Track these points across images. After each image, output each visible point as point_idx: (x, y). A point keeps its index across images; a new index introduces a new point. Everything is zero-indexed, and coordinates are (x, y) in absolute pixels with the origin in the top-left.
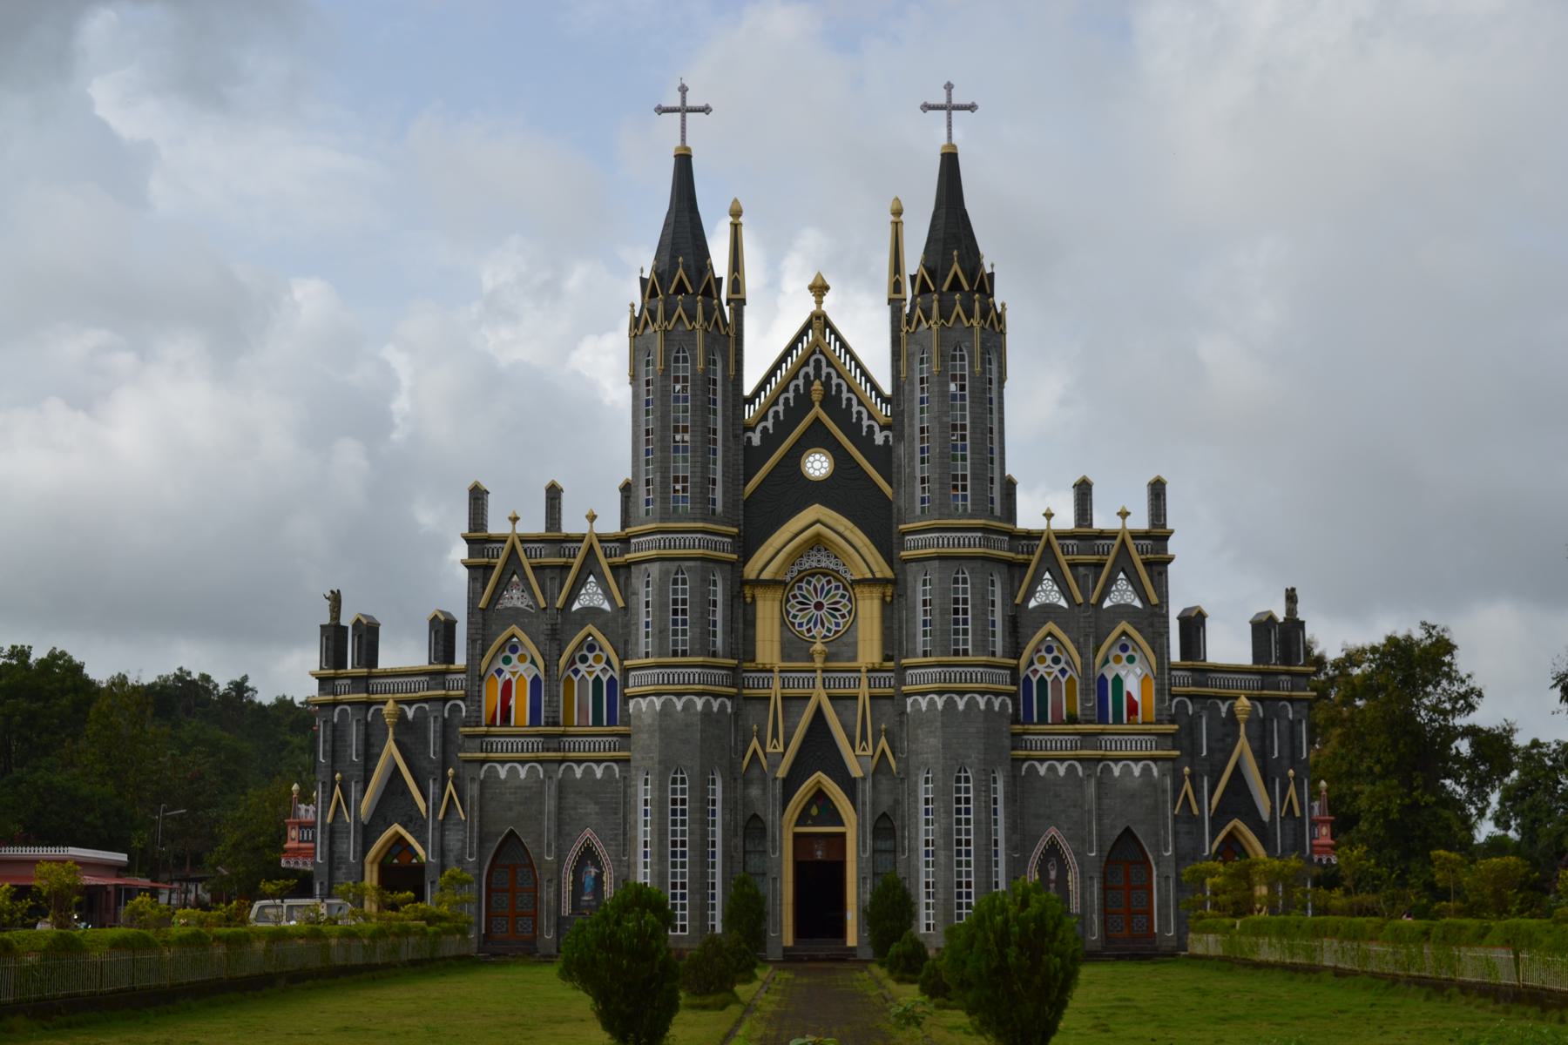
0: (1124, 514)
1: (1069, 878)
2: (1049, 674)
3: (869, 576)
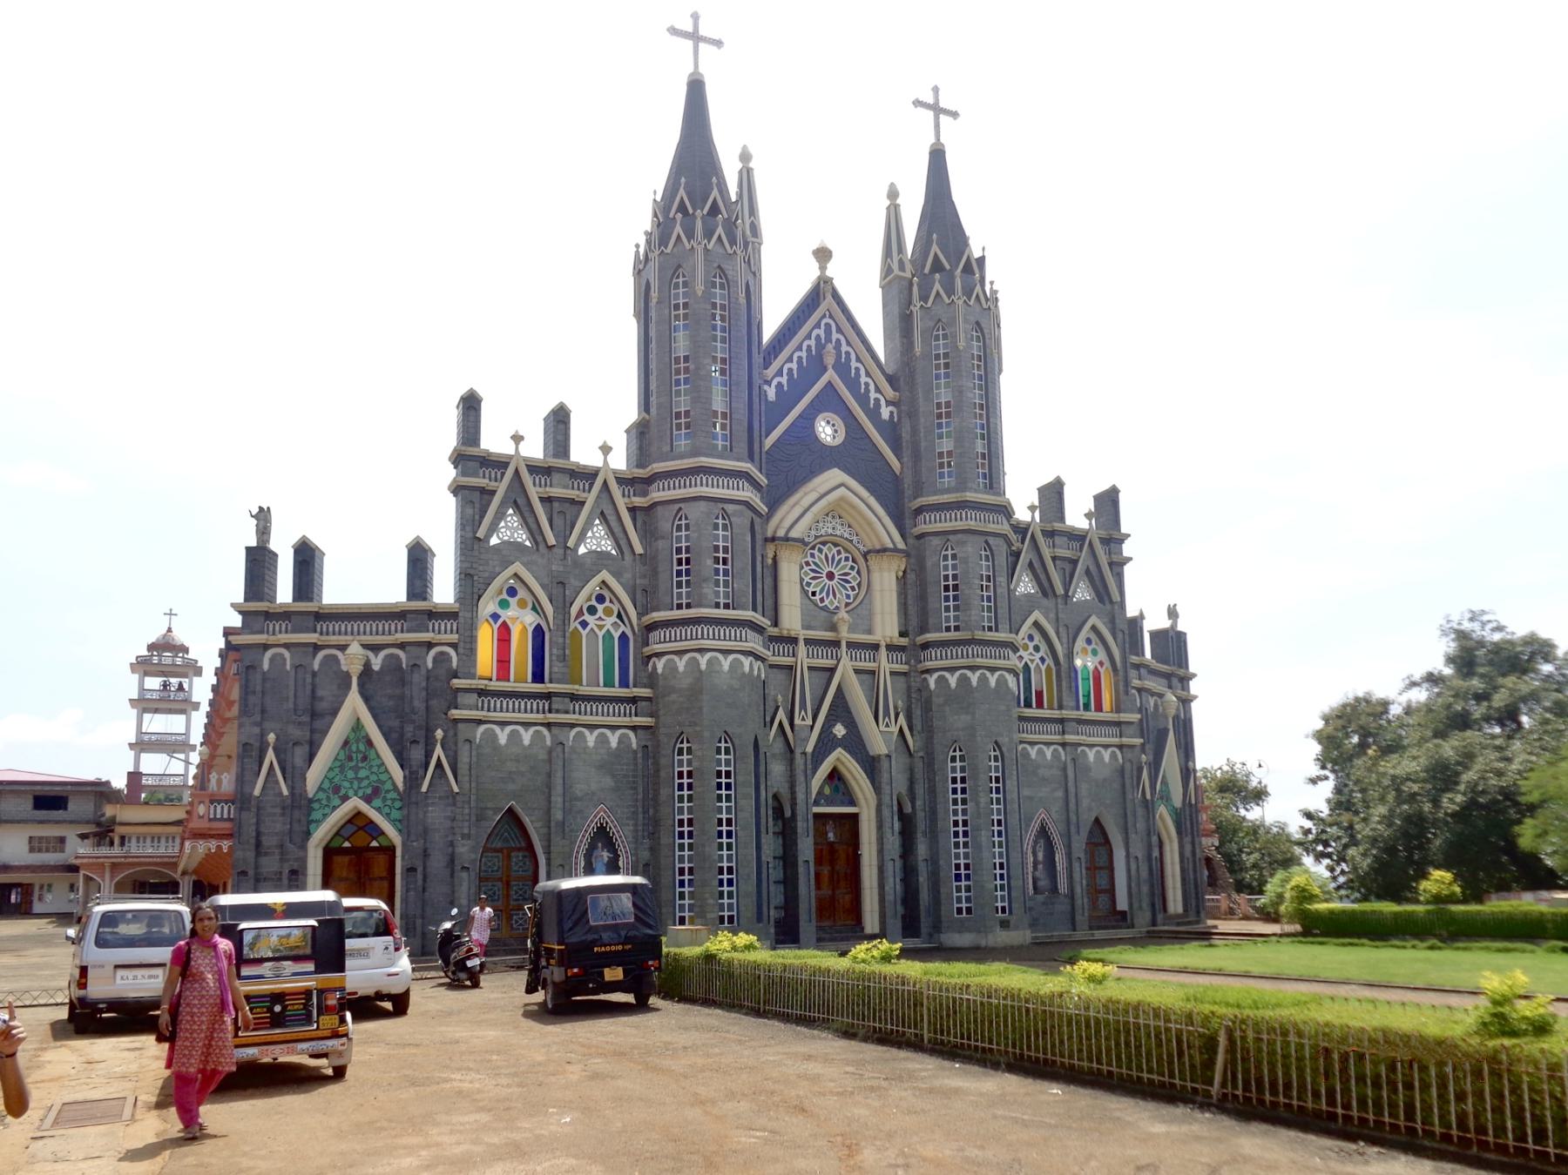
0: (517, 439)
1: (1057, 859)
2: (1032, 661)
3: (891, 546)
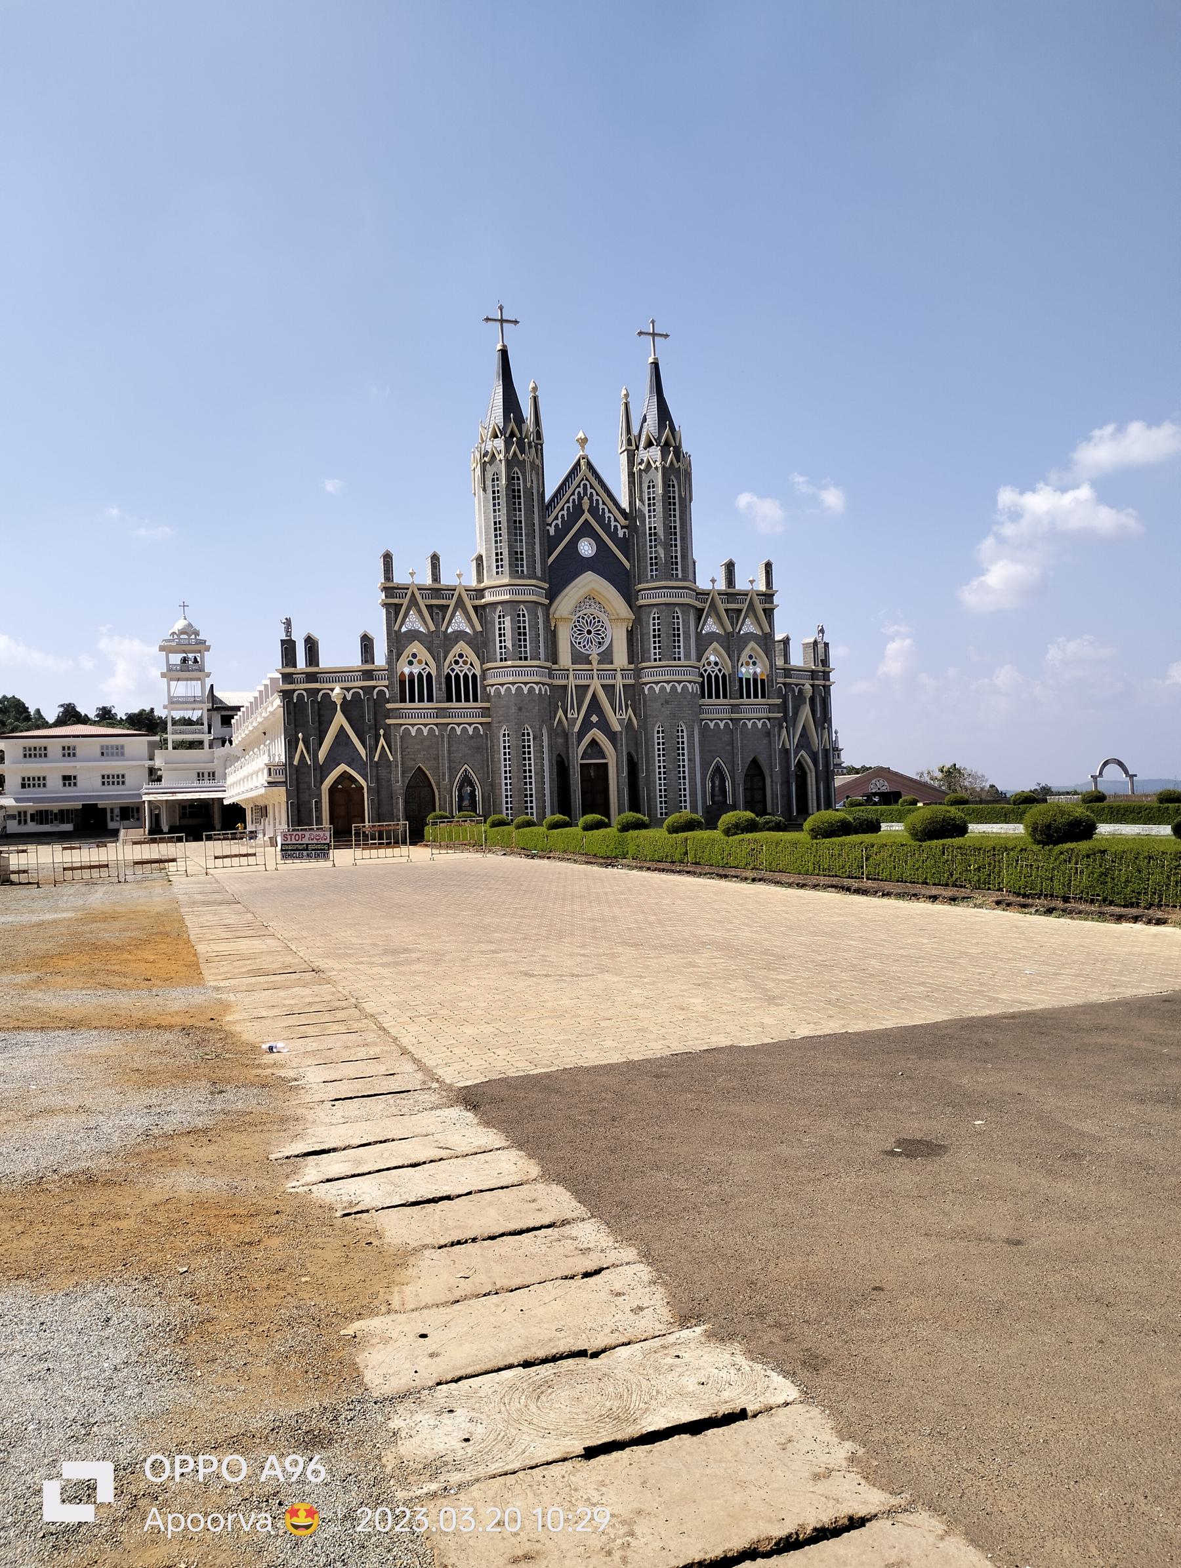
0: (713, 581)
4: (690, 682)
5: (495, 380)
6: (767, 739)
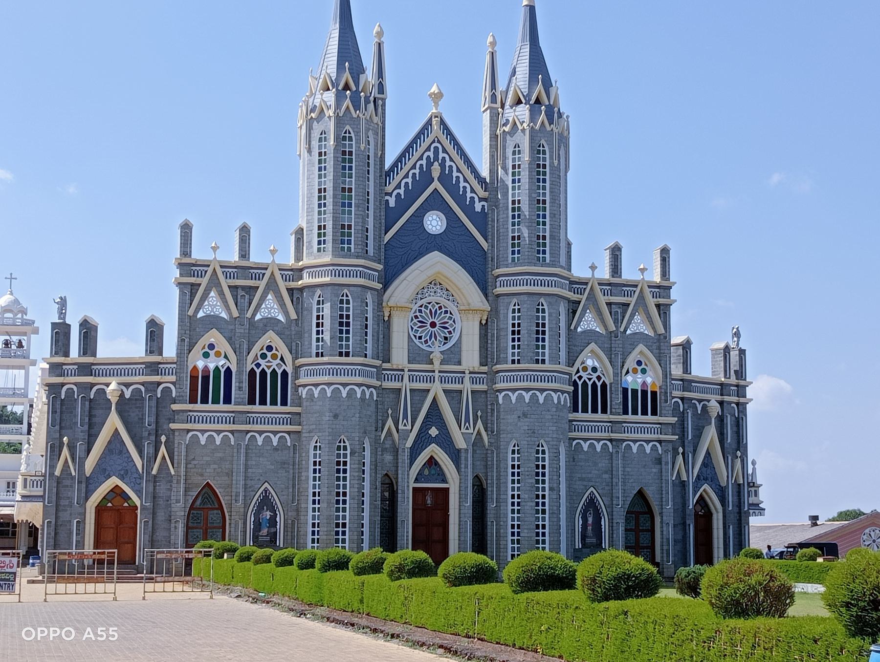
0: (593, 268)
2: (590, 379)
4: (555, 391)
5: (332, 22)
6: (658, 466)
